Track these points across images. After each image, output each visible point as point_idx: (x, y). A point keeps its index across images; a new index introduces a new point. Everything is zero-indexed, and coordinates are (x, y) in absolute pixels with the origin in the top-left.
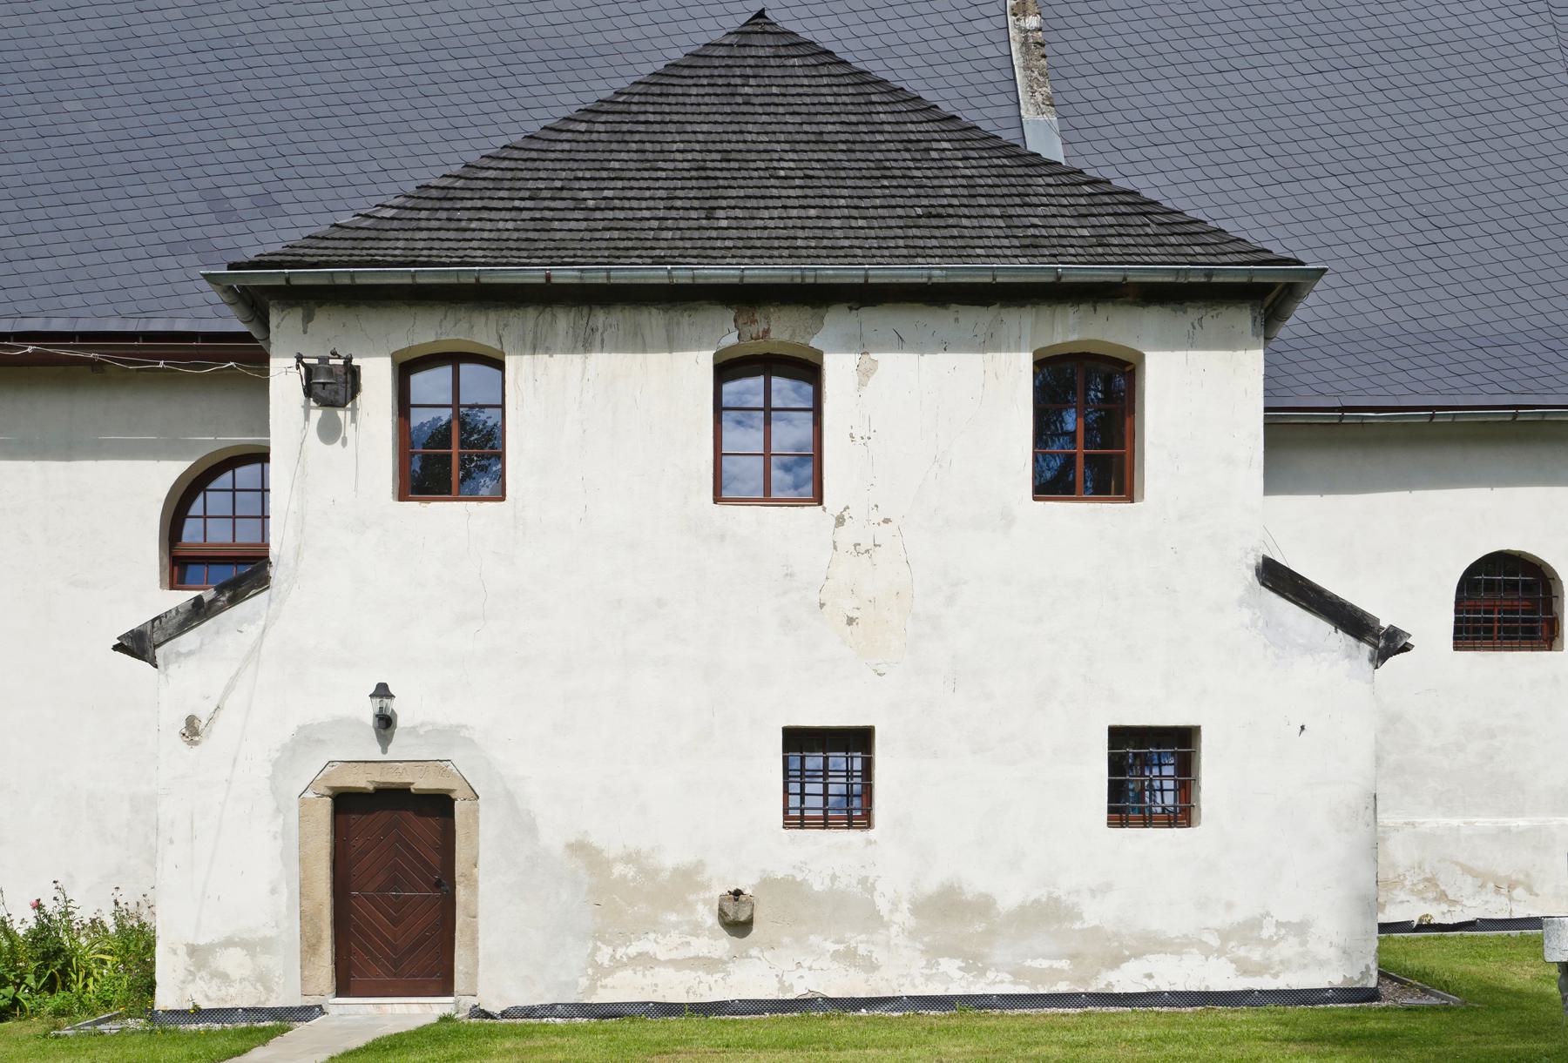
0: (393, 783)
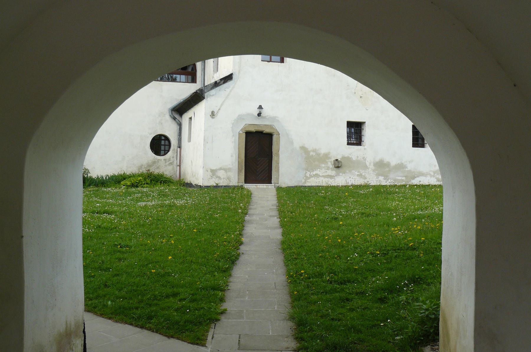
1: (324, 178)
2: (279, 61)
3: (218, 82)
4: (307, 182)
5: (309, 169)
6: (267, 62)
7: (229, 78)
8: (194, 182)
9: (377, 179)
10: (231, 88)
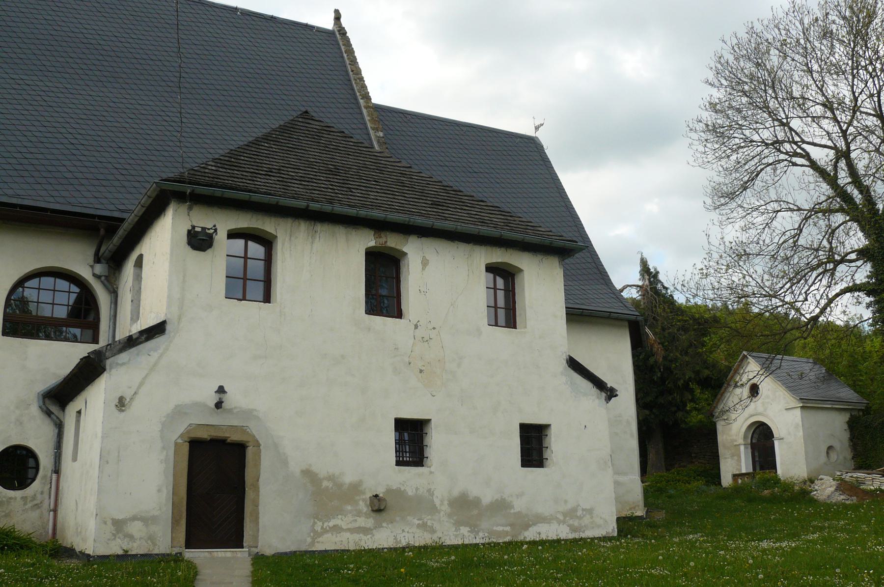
1: (352, 534)
2: (262, 300)
3: (134, 337)
4: (317, 542)
5: (320, 516)
7: (158, 329)
8: (79, 546)
9: (455, 533)
10: (160, 351)
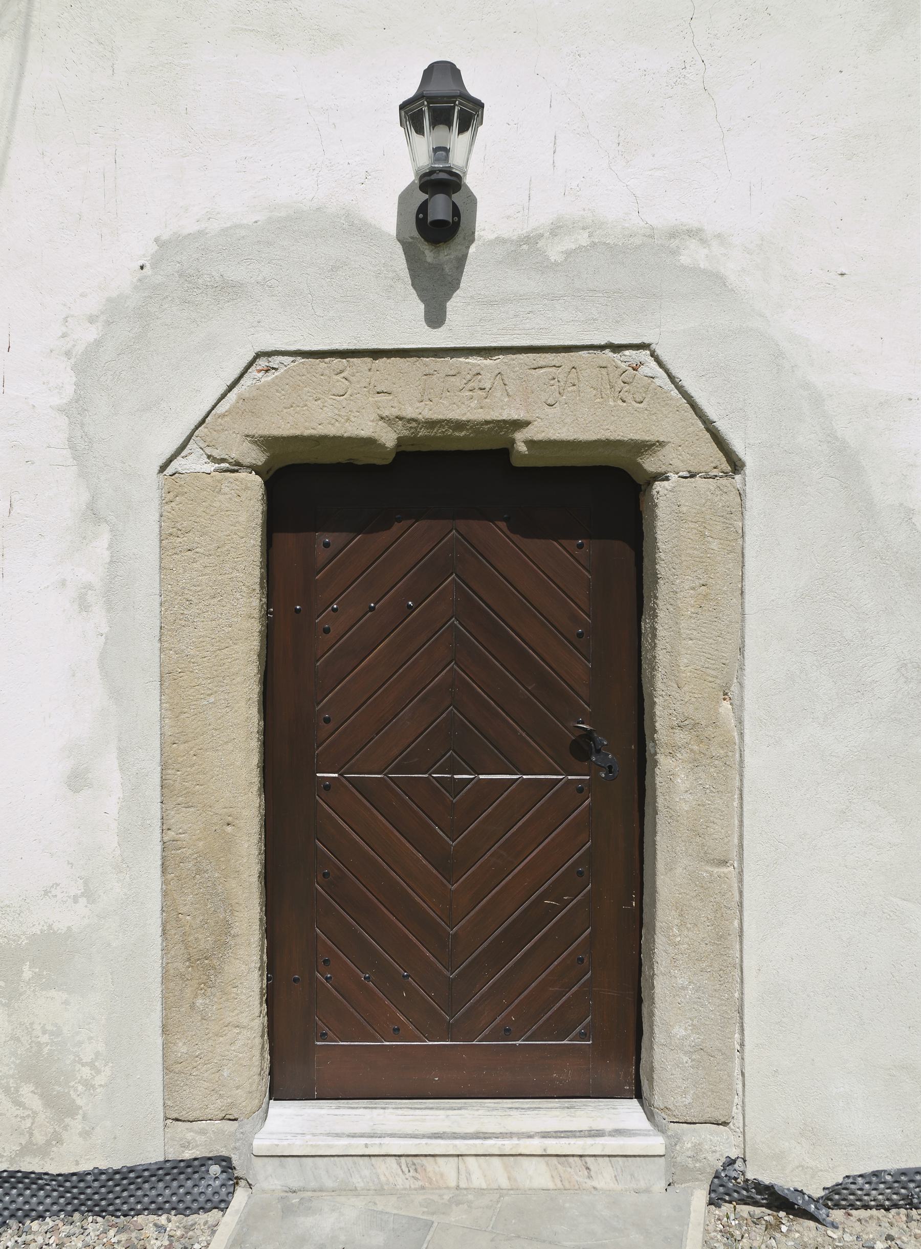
0: (459, 425)
6: (368, 360)
